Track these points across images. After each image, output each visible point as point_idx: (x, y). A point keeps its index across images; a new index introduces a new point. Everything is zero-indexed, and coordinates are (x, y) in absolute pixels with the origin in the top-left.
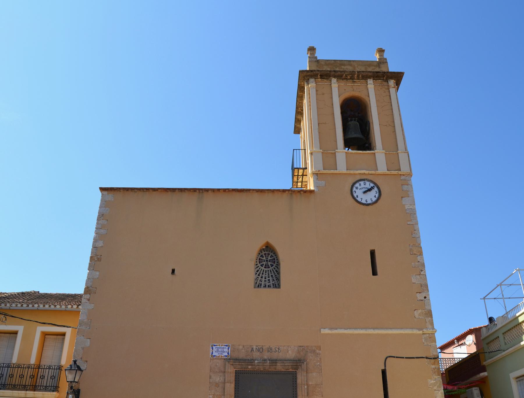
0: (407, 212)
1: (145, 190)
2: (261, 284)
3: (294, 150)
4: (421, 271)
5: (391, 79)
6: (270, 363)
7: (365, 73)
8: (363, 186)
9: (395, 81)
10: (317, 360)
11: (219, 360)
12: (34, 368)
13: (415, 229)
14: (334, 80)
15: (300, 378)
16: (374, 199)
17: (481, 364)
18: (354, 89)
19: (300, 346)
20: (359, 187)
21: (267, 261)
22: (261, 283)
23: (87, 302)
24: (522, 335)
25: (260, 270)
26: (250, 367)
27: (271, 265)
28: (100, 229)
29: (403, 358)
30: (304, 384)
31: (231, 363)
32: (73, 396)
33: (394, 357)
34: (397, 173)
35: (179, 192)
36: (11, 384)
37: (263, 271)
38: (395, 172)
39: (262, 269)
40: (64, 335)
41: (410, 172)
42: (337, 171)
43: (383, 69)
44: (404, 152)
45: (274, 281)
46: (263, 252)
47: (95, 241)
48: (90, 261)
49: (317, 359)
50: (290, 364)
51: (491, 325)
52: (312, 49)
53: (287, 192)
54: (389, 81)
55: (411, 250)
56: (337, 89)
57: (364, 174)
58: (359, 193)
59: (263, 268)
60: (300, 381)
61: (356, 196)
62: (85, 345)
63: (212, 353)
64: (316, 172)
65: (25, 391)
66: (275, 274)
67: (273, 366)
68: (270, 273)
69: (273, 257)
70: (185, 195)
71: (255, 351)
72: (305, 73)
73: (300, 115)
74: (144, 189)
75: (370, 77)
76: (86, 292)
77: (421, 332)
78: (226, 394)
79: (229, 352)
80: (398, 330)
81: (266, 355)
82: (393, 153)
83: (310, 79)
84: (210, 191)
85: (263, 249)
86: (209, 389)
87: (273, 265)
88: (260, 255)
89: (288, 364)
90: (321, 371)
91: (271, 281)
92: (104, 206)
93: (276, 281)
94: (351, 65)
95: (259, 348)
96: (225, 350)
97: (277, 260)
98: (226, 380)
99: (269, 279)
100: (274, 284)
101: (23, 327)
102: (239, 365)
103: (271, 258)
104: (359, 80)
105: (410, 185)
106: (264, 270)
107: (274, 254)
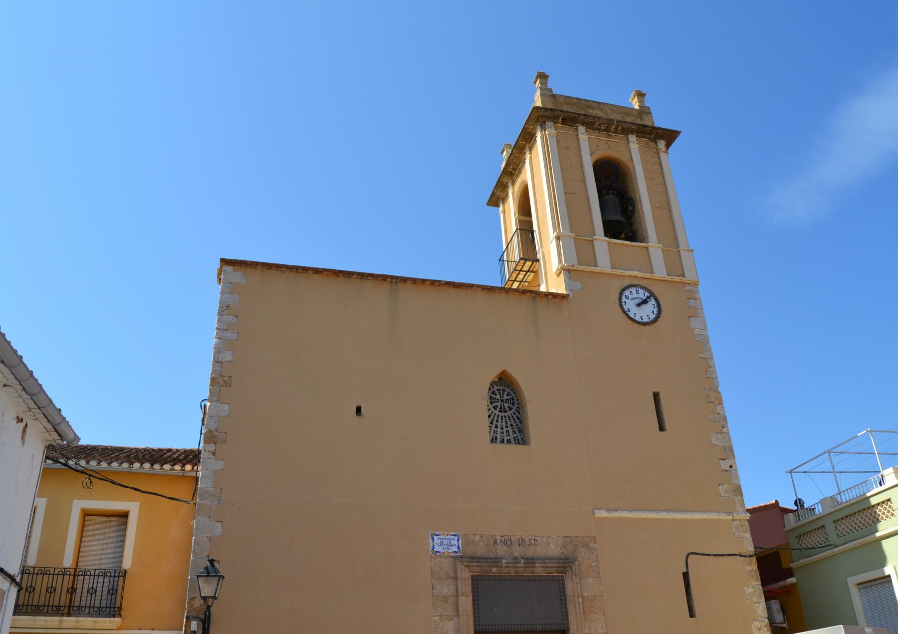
0: (697, 339)
1: (301, 271)
2: (496, 437)
6: (524, 563)
8: (635, 295)
9: (665, 143)
10: (591, 558)
11: (445, 558)
12: (94, 576)
14: (582, 129)
15: (571, 586)
16: (652, 317)
17: (782, 565)
18: (610, 147)
19: (566, 537)
20: (630, 297)
21: (502, 401)
23: (212, 456)
24: (876, 523)
26: (494, 570)
27: (508, 407)
28: (224, 330)
29: (710, 555)
30: (578, 596)
31: (465, 564)
32: (198, 624)
36: (51, 604)
37: (498, 417)
38: (678, 278)
39: (495, 414)
40: (125, 515)
43: (647, 122)
45: (515, 433)
46: (495, 386)
47: (218, 350)
48: (211, 385)
49: (592, 557)
50: (554, 565)
51: (802, 511)
53: (528, 294)
54: (658, 142)
55: (707, 395)
56: (587, 143)
57: (636, 277)
59: (497, 412)
60: (572, 591)
61: (626, 310)
62: (213, 533)
63: (433, 548)
64: (568, 268)
65: (59, 616)
66: (516, 422)
67: (529, 567)
68: (508, 420)
69: (511, 395)
70: (369, 284)
71: (499, 544)
73: (509, 176)
74: (300, 269)
75: (632, 132)
76: (208, 439)
77: (730, 517)
78: (461, 614)
79: (460, 546)
80: (701, 513)
81: (517, 551)
82: (672, 249)
83: (547, 122)
84: (410, 282)
85: (495, 382)
86: (433, 607)
88: (490, 392)
89: (552, 565)
90: (599, 576)
91: (511, 433)
92: (229, 291)
93: (518, 434)
94: (602, 110)
95: (506, 540)
96: (453, 542)
97: (517, 400)
99: (508, 431)
100: (516, 438)
101: (46, 499)
102: (478, 566)
103: (509, 397)
104: (617, 133)
106: (498, 415)
107: (512, 390)
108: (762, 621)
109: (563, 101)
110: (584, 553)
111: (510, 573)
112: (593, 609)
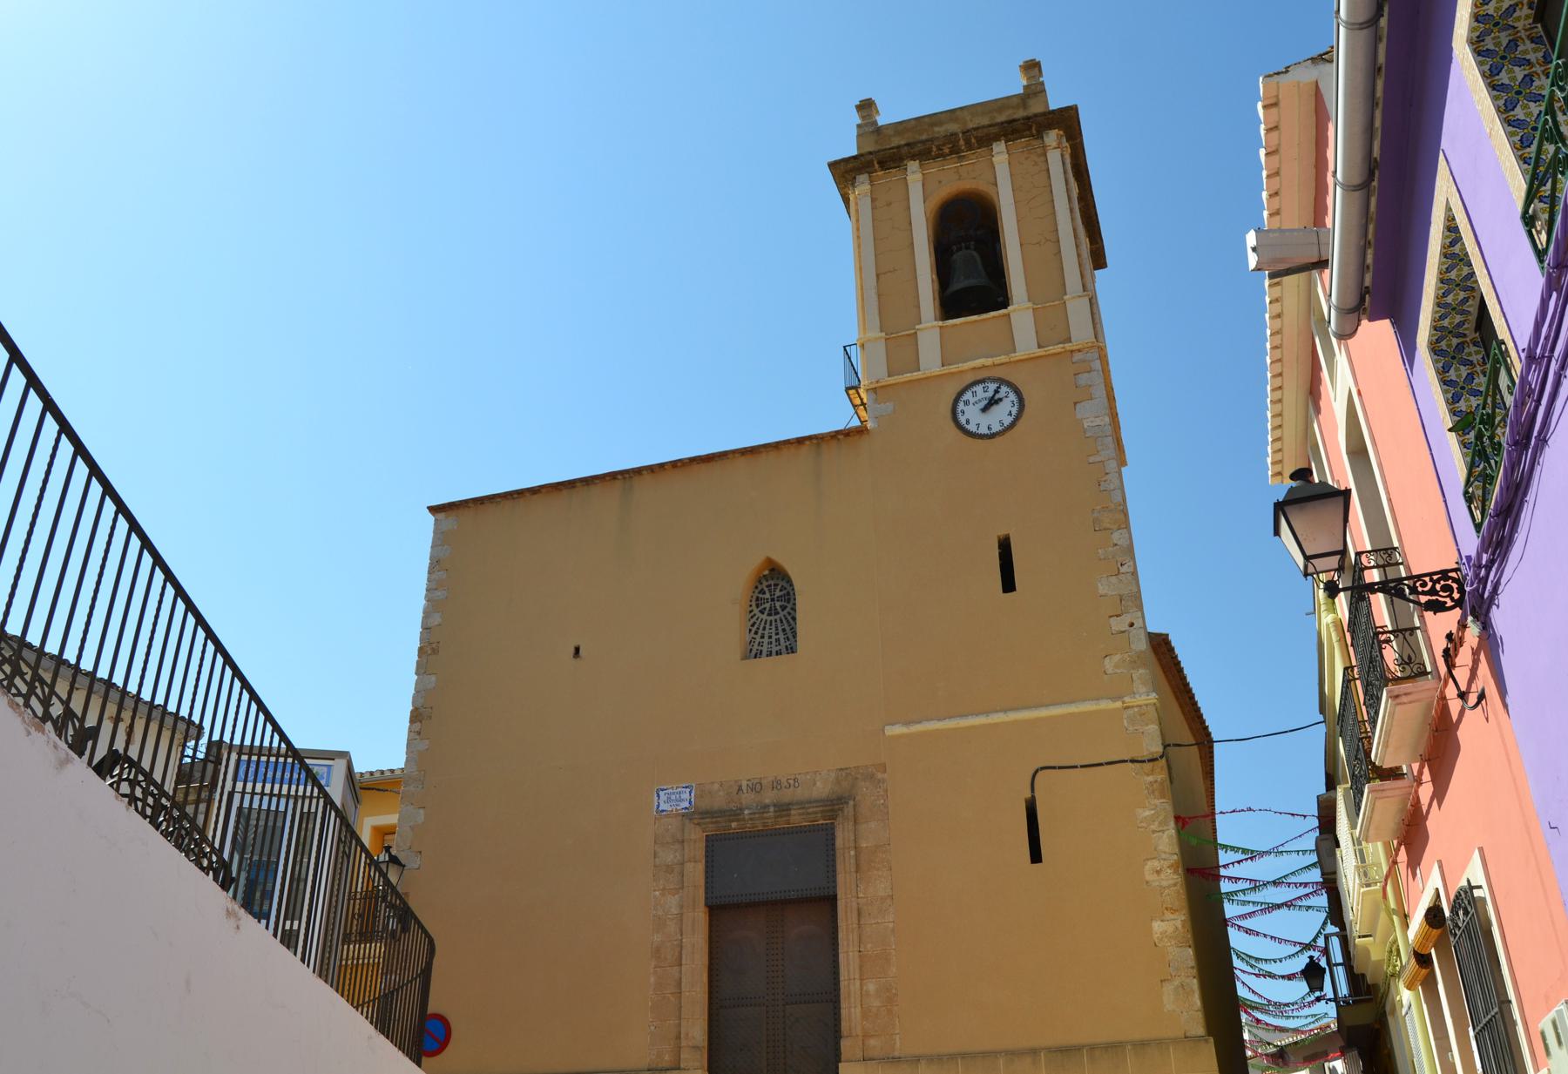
2: (761, 651)
3: (844, 347)
4: (1122, 565)
5: (1051, 129)
6: (775, 811)
7: (980, 131)
13: (1107, 471)
18: (960, 176)
19: (841, 769)
20: (972, 400)
21: (773, 600)
22: (760, 648)
23: (417, 737)
25: (758, 622)
26: (734, 825)
27: (781, 606)
29: (1076, 767)
31: (696, 821)
33: (1054, 768)
34: (1063, 350)
35: (584, 485)
37: (765, 624)
38: (1056, 347)
39: (762, 620)
41: (1095, 340)
42: (920, 373)
43: (1035, 108)
44: (1080, 296)
45: (788, 640)
47: (427, 614)
50: (818, 809)
52: (866, 107)
57: (984, 366)
58: (972, 415)
59: (764, 617)
63: (658, 806)
64: (873, 386)
69: (785, 589)
70: (595, 490)
71: (745, 791)
72: (842, 167)
75: (997, 138)
79: (692, 800)
81: (769, 797)
85: (764, 576)
87: (786, 607)
88: (757, 591)
89: (815, 809)
91: (782, 641)
94: (956, 120)
96: (683, 796)
98: (686, 857)
102: (712, 823)
103: (782, 593)
105: (1094, 371)
108: (1164, 860)
109: (892, 133)
110: (867, 789)
111: (757, 827)
112: (873, 865)
